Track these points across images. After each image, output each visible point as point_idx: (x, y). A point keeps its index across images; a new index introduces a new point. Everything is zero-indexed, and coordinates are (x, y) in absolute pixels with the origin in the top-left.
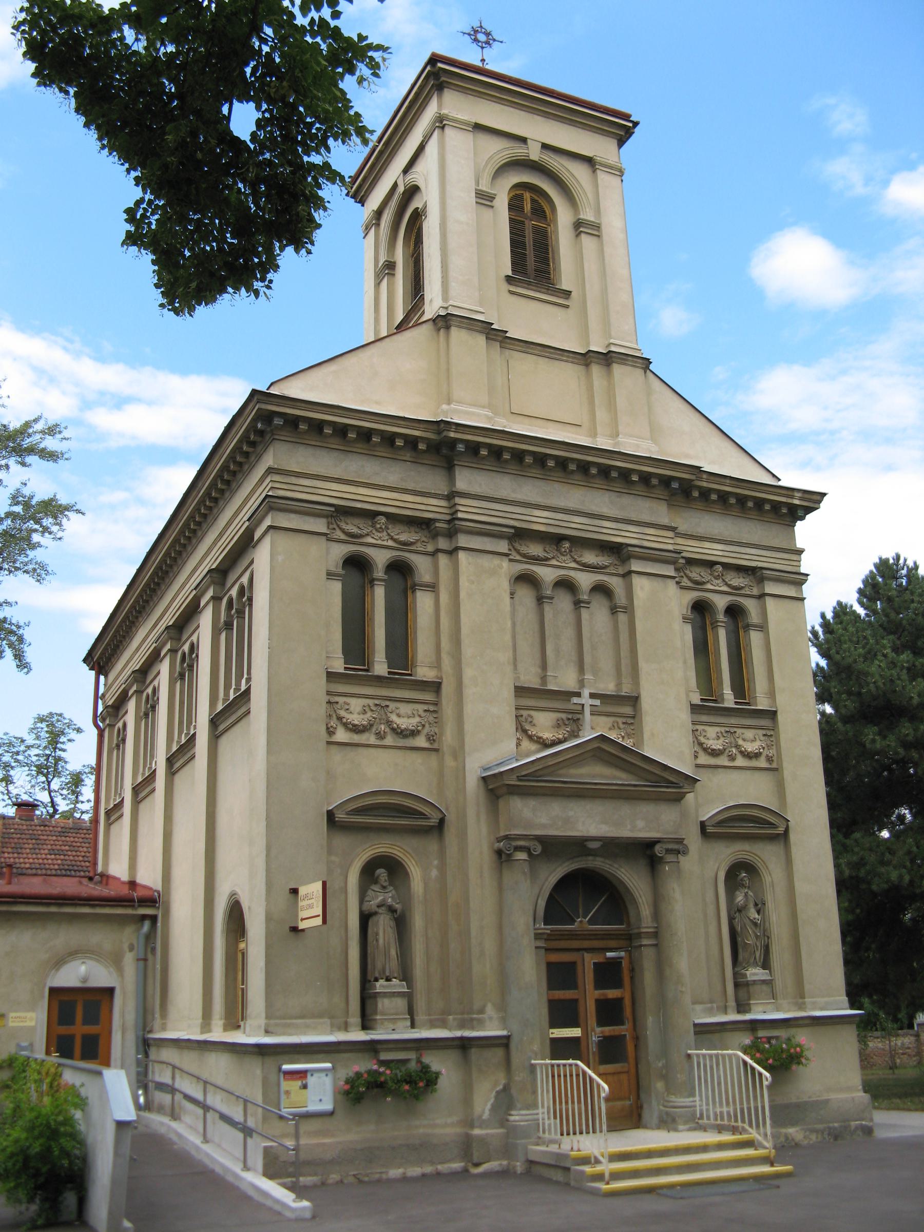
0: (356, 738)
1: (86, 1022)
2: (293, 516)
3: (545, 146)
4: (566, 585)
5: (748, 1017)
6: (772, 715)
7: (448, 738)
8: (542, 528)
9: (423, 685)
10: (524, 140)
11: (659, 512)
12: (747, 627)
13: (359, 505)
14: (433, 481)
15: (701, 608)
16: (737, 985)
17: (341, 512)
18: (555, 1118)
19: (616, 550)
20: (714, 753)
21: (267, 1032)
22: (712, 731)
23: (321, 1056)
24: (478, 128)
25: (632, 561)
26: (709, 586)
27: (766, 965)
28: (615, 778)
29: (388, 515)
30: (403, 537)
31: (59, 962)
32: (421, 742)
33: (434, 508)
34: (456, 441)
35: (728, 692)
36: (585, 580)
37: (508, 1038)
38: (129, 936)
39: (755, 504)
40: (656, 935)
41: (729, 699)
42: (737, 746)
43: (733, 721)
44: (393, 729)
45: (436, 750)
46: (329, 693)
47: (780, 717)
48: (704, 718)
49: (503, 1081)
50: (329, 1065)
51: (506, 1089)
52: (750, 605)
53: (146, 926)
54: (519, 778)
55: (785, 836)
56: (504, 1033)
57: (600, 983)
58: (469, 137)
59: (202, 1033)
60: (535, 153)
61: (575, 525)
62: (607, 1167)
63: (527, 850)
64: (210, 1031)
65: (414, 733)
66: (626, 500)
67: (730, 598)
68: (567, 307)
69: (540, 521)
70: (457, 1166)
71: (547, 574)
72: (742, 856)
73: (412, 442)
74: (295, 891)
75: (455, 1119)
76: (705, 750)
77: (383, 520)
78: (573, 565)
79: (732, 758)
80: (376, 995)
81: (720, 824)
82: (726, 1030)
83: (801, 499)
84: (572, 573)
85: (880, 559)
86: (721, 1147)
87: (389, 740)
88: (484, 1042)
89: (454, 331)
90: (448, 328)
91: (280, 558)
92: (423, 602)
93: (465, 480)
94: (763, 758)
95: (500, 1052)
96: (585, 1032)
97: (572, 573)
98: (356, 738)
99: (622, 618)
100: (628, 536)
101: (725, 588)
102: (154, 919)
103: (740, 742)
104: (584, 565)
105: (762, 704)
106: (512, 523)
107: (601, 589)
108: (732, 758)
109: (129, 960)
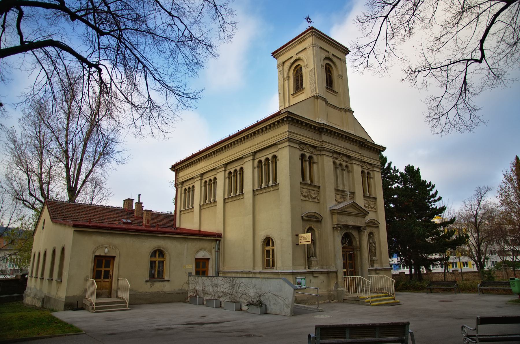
0: (305, 199)
1: (202, 268)
2: (292, 143)
3: (333, 55)
4: (341, 165)
5: (374, 268)
6: (376, 198)
7: (322, 200)
8: (338, 151)
9: (316, 187)
10: (328, 52)
11: (355, 148)
12: (314, 163)
13: (304, 142)
14: (316, 136)
15: (303, 156)
16: (308, 261)
17: (301, 143)
18: (366, 288)
19: (349, 157)
20: (305, 197)
21: (293, 269)
22: (305, 190)
23: (303, 275)
24: (321, 48)
25: (375, 168)
26: (364, 167)
27: (316, 256)
28: (354, 211)
29: (367, 163)
30: (311, 150)
31: (198, 252)
32: (316, 200)
33: (317, 144)
34: (324, 128)
35: (308, 179)
36: (344, 164)
37: (337, 271)
38: (214, 244)
39: (296, 121)
40: (360, 248)
41: (309, 182)
42: (311, 195)
43: (369, 199)
44: (311, 197)
45: (319, 203)
46: (301, 188)
47: (377, 199)
48: (338, 193)
49: (336, 281)
50: (304, 277)
51: (337, 283)
52: (371, 172)
53: (218, 242)
54: (340, 211)
55: (378, 227)
56: (337, 270)
57: (159, 262)
58: (319, 49)
59: (253, 270)
60: (331, 56)
61: (344, 151)
62: (370, 300)
63: (340, 227)
64: (255, 270)
65: (315, 198)
66: (352, 146)
67: (310, 154)
68: (337, 96)
69: (338, 149)
70: (328, 301)
71: (338, 162)
72: (371, 231)
73: (315, 127)
74: (297, 235)
75: (326, 290)
76: (303, 195)
77: (308, 146)
78: (342, 160)
79: (369, 208)
80: (312, 261)
81: (306, 217)
82: (371, 271)
83: (382, 149)
84: (342, 162)
85: (405, 167)
86: (383, 296)
87: (310, 200)
88: (333, 272)
89: (319, 100)
90: (317, 99)
91: (291, 153)
92: (315, 166)
93: (325, 138)
94: (374, 209)
95: (335, 275)
96: (347, 270)
97: (342, 162)
98: (305, 199)
99: (351, 174)
100: (352, 154)
101: (309, 152)
102: (220, 241)
103: (311, 194)
104: (344, 161)
105: (374, 196)
106: (333, 149)
107: (347, 166)
108: (369, 208)
109: (213, 251)
